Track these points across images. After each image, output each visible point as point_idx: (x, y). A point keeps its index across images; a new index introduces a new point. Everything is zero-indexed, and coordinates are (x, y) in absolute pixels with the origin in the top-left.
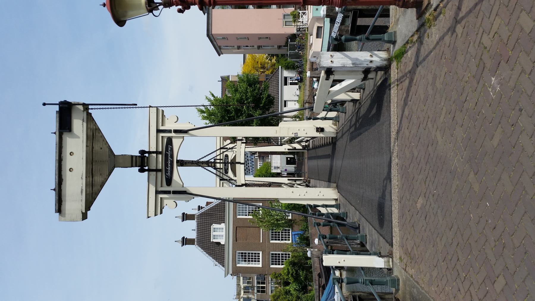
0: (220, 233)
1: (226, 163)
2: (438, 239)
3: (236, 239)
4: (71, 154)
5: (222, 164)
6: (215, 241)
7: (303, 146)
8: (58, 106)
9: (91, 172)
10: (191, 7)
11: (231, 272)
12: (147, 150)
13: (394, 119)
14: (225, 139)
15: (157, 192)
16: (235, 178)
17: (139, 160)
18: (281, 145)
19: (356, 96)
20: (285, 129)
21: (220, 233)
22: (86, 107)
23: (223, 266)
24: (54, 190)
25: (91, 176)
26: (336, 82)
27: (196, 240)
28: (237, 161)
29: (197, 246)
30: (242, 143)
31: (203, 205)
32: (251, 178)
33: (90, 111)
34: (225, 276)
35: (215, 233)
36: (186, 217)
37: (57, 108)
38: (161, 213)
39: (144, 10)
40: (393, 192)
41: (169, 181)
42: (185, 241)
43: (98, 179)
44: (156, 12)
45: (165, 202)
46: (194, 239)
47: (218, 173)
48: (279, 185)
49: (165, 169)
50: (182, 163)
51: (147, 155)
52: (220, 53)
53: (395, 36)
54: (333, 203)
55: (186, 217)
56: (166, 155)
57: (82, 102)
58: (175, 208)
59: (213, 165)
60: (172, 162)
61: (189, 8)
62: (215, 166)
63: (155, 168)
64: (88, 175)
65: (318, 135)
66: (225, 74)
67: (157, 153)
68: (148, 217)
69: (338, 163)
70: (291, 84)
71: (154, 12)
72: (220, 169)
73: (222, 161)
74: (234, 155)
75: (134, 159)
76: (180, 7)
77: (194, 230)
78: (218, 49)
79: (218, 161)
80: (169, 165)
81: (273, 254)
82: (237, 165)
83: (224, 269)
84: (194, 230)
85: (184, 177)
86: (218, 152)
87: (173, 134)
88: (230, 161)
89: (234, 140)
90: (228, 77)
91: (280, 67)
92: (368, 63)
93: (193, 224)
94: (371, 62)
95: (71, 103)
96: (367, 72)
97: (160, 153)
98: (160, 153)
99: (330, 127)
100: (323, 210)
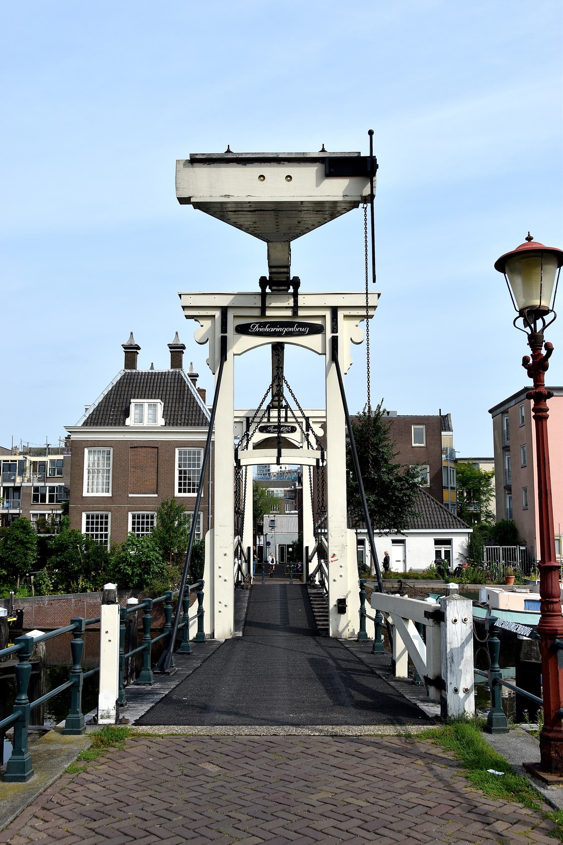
0: (147, 416)
1: (278, 428)
2: (151, 793)
3: (135, 446)
4: (289, 178)
5: (276, 420)
6: (132, 407)
7: (314, 575)
8: (368, 155)
9: (259, 208)
10: (532, 379)
11: (74, 437)
12: (300, 290)
13: (355, 730)
14: (324, 426)
15: (224, 310)
16: (250, 446)
17: (282, 278)
18: (316, 534)
19: (402, 671)
20: (342, 538)
21: (147, 416)
22: (369, 198)
23: (86, 424)
24: (228, 151)
25: (251, 209)
26: (420, 628)
27: (134, 371)
28: (283, 450)
29: (123, 373)
30: (318, 460)
31: (200, 384)
32: (251, 475)
33: (361, 205)
34: (66, 428)
35: (146, 405)
36: (177, 352)
37: (365, 153)
38: (188, 317)
39: (523, 303)
40: (229, 727)
41: (243, 330)
42: (131, 352)
43: (247, 219)
44: (521, 320)
45: (207, 323)
46: (135, 368)
47: (260, 414)
48: (239, 531)
49: (266, 323)
50: (278, 349)
51: (291, 290)
52: (495, 413)
53: (499, 731)
54: (207, 630)
55: (177, 352)
56: (291, 324)
57: (377, 192)
58: (196, 338)
59: (276, 403)
60: (279, 334)
61: (530, 375)
62: (274, 407)
63: (267, 304)
64: (254, 205)
65: (333, 602)
66: (454, 423)
67: (295, 308)
68: (180, 295)
69: (281, 639)
70: (438, 553)
71: (521, 319)
72: (269, 417)
73: (282, 420)
74: (297, 444)
75: (285, 270)
76: (531, 362)
77: (152, 368)
78: (502, 409)
79: (283, 414)
80: (273, 330)
81: (107, 517)
82: (275, 451)
83: (80, 424)
84: (152, 368)
85: (251, 357)
86: (298, 414)
87: (329, 335)
88: (283, 435)
89: (322, 444)
90: (450, 429)
91: (471, 531)
92: (454, 685)
93: (164, 365)
94: (456, 691)
95: (374, 175)
96: (440, 683)
97: (295, 314)
98: (295, 314)
99: (347, 625)
100: (193, 611)
